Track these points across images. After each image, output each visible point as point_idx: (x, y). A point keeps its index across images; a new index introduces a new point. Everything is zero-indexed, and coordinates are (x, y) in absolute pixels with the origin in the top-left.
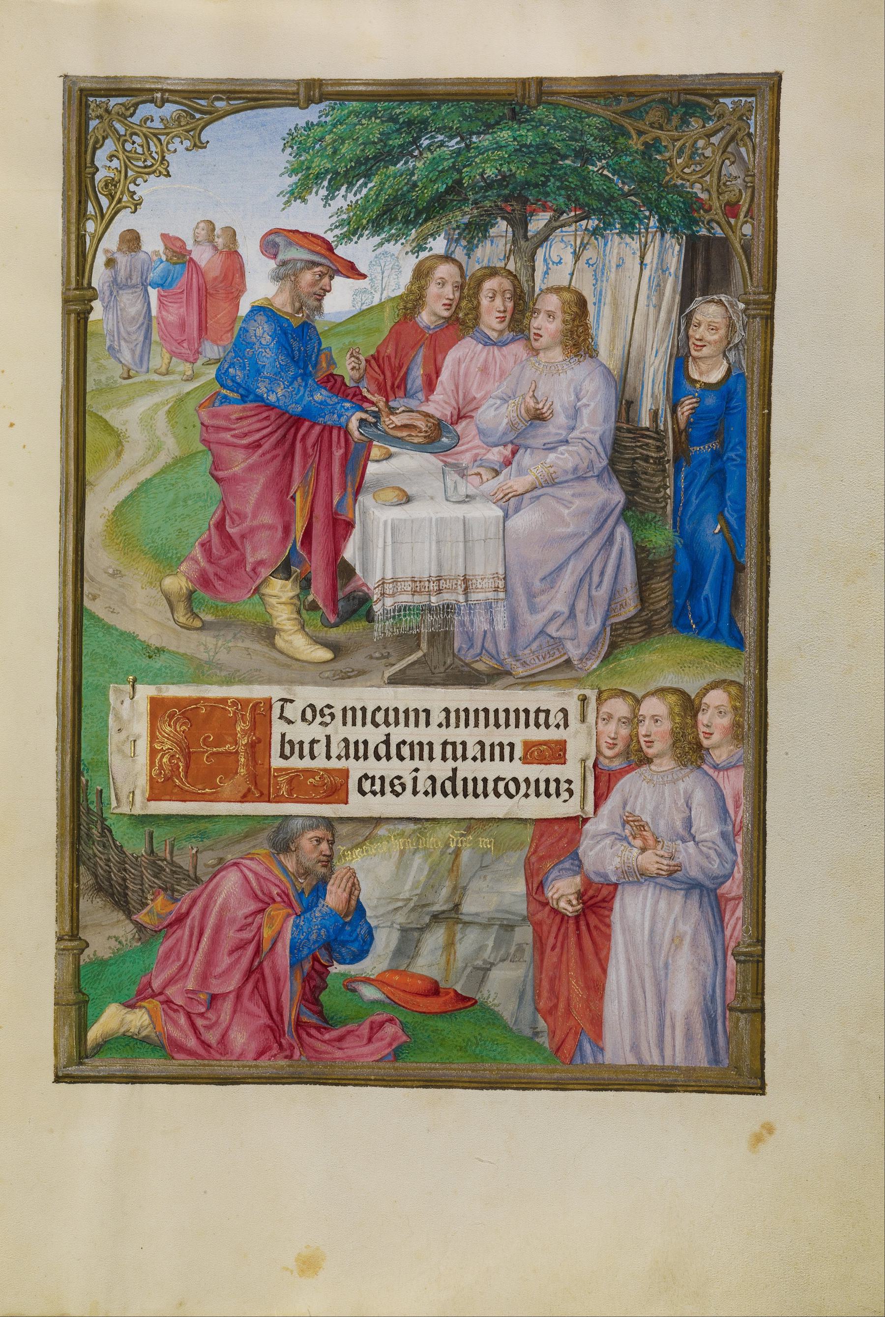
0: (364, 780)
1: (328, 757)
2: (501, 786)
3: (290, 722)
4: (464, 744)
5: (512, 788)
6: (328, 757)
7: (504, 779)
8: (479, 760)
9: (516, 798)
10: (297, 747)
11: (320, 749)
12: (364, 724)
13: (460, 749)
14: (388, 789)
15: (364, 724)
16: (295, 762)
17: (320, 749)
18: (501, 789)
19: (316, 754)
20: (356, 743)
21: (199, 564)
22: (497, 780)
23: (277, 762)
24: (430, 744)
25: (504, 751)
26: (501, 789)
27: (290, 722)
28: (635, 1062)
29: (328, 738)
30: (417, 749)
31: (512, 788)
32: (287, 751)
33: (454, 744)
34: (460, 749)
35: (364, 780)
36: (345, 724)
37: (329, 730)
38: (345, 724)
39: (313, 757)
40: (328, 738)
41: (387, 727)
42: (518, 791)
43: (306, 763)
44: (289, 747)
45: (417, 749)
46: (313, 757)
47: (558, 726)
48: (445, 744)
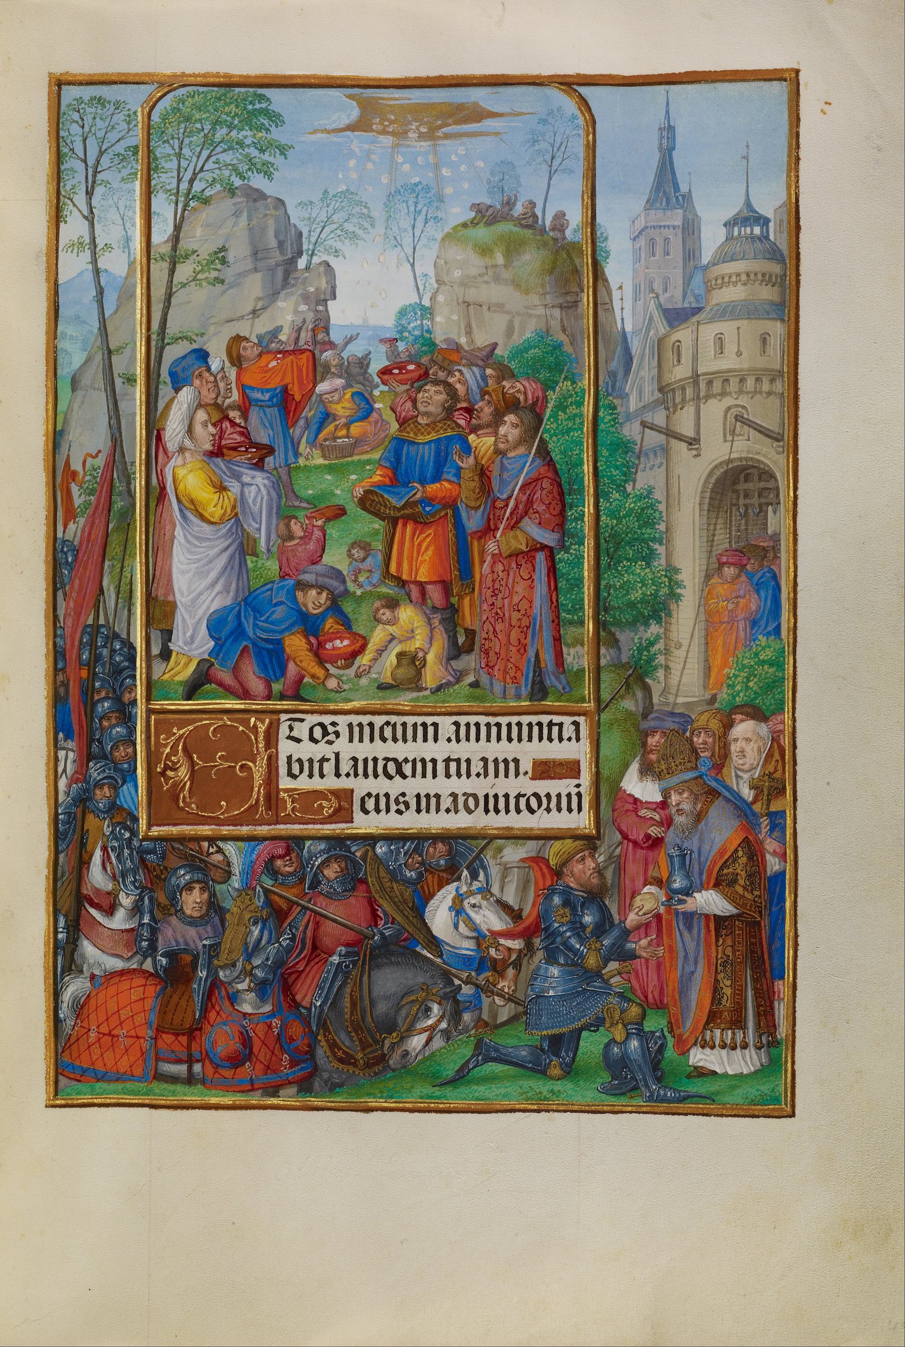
0: (367, 798)
1: (338, 775)
2: (523, 801)
3: (298, 741)
4: (468, 761)
5: (534, 803)
6: (338, 775)
7: (524, 795)
8: (482, 776)
9: (537, 815)
10: (306, 765)
11: (329, 767)
12: (372, 740)
13: (464, 766)
14: (393, 807)
15: (372, 740)
16: (304, 783)
17: (329, 767)
18: (523, 805)
19: (325, 773)
20: (366, 761)
21: (420, 298)
22: (518, 796)
23: (285, 783)
24: (434, 761)
25: (510, 766)
26: (523, 805)
27: (298, 741)
28: (290, 983)
29: (337, 755)
30: (419, 766)
31: (534, 803)
32: (296, 769)
33: (458, 761)
34: (464, 766)
35: (367, 798)
36: (351, 740)
37: (336, 747)
38: (351, 740)
39: (322, 776)
40: (337, 755)
41: (395, 742)
42: (540, 806)
43: (316, 784)
44: (295, 767)
45: (419, 766)
46: (322, 776)
47: (569, 739)
48: (448, 761)
